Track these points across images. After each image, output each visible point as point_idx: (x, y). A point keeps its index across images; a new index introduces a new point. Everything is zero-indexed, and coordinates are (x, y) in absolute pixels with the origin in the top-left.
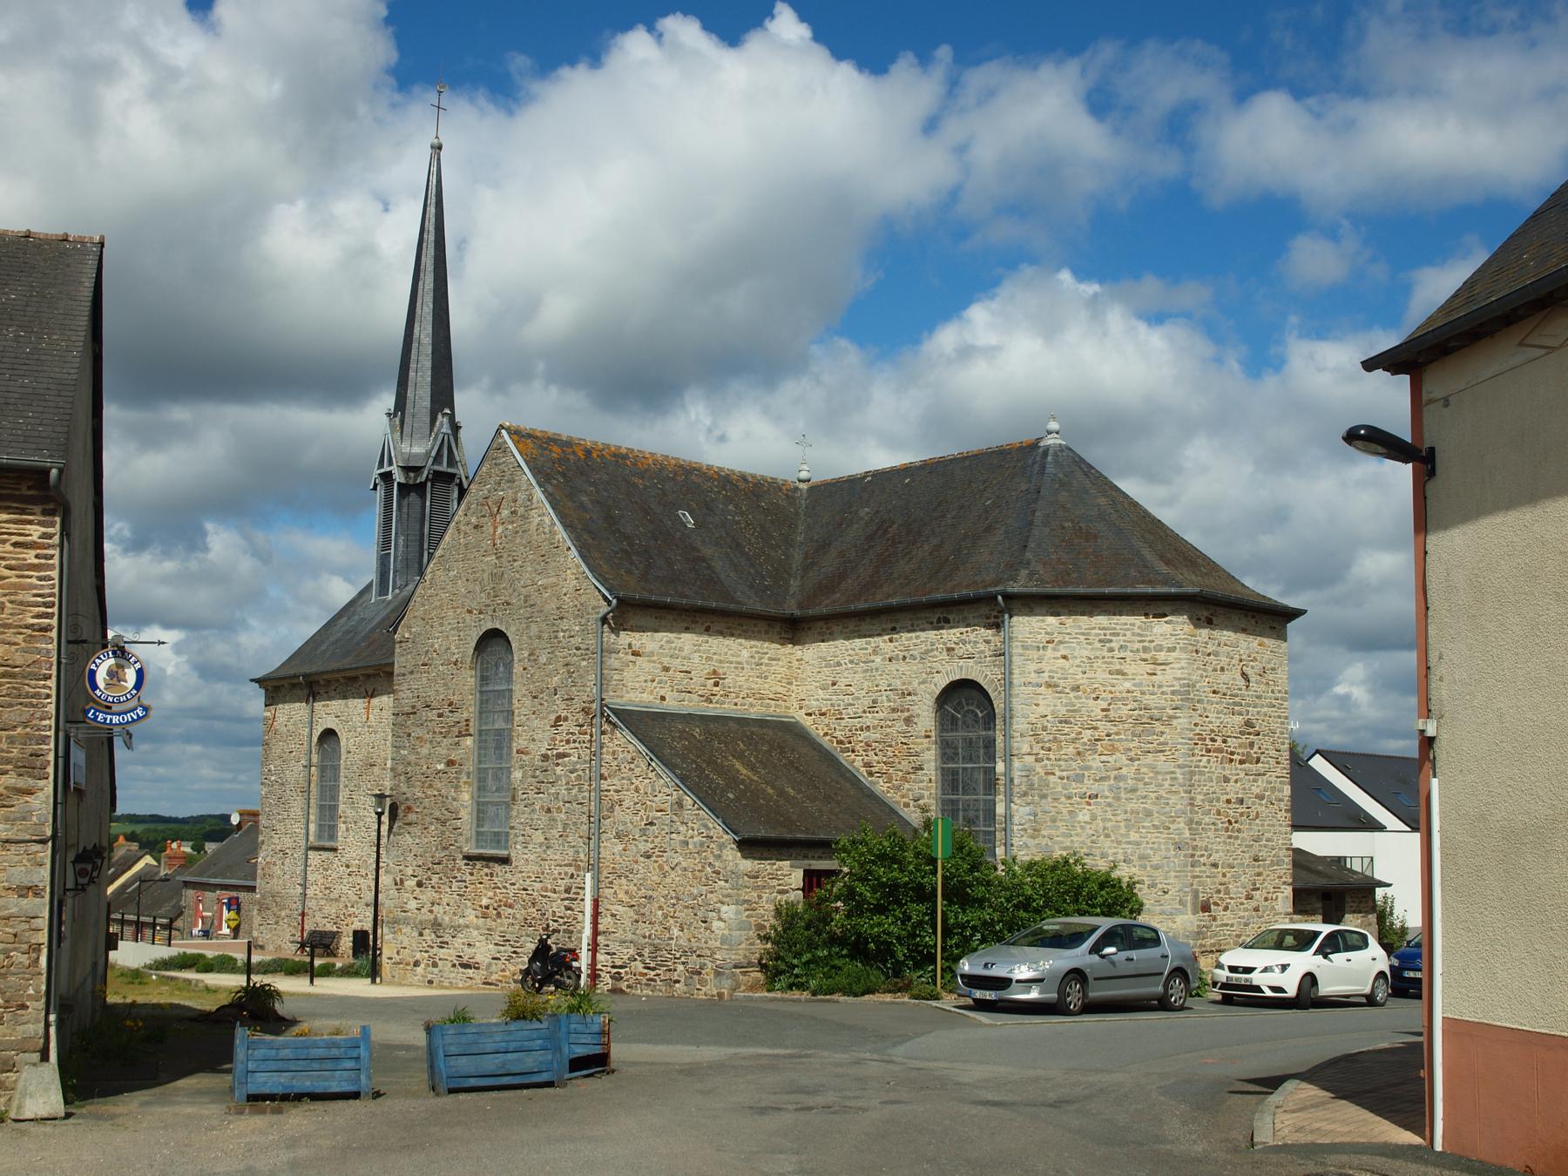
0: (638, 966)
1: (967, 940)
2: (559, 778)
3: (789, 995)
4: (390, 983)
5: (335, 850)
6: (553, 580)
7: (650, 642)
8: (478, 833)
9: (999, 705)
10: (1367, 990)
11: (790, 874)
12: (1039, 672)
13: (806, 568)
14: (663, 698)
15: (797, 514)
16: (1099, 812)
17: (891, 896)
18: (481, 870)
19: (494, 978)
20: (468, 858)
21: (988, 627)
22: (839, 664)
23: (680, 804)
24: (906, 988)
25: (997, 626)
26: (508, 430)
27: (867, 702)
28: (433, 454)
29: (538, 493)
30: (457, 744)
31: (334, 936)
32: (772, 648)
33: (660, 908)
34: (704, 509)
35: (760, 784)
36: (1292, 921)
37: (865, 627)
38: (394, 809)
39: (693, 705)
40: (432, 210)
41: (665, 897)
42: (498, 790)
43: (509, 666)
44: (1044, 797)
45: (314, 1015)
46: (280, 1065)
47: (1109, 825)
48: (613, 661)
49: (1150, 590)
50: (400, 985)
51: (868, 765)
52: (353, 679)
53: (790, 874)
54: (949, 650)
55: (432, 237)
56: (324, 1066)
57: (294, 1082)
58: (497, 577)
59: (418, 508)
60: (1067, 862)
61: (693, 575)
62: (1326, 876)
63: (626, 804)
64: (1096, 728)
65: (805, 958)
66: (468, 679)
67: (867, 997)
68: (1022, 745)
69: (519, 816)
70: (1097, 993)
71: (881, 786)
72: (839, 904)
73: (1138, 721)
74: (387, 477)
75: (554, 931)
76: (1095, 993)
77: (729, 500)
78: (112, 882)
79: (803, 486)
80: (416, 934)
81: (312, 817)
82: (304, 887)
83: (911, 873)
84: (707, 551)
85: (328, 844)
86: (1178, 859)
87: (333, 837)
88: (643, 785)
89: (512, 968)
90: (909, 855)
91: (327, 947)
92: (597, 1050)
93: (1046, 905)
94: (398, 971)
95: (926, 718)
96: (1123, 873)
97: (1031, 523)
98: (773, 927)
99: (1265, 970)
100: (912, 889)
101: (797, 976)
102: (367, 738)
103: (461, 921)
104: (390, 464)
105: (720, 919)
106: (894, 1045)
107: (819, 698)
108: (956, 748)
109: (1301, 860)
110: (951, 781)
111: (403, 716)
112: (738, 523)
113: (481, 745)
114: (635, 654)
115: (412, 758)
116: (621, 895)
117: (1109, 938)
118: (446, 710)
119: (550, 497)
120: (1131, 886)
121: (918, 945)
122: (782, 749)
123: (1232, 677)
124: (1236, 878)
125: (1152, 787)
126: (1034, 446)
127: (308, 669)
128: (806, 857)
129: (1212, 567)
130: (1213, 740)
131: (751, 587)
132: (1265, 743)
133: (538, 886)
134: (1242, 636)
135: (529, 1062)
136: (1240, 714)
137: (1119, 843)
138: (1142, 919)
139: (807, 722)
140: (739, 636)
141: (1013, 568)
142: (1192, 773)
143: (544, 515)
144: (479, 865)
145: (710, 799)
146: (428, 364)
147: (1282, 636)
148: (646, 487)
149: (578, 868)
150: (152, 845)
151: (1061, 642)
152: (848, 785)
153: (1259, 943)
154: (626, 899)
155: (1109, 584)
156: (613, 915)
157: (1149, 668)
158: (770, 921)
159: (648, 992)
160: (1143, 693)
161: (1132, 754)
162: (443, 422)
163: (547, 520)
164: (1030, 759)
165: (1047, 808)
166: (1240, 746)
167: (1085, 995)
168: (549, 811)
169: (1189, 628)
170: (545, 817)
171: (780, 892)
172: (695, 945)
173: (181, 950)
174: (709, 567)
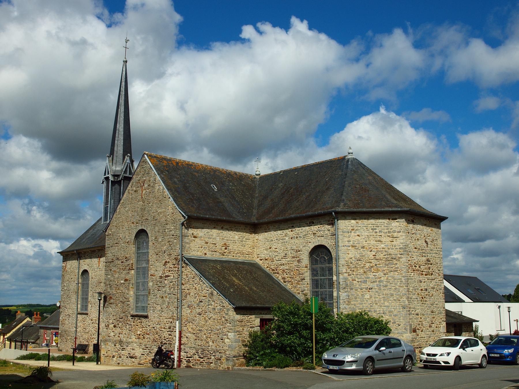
0: (197, 357)
1: (324, 345)
2: (166, 285)
3: (254, 368)
4: (104, 364)
5: (87, 314)
6: (164, 210)
7: (201, 232)
8: (136, 307)
9: (334, 254)
10: (479, 362)
11: (255, 321)
12: (349, 241)
13: (259, 206)
14: (205, 254)
15: (255, 186)
16: (373, 295)
17: (295, 329)
18: (138, 321)
19: (142, 362)
20: (133, 316)
21: (329, 224)
22: (272, 241)
23: (212, 294)
24: (301, 365)
25: (332, 224)
26: (147, 155)
27: (283, 254)
28: (124, 170)
29: (158, 178)
31: (86, 346)
32: (247, 235)
33: (205, 334)
35: (243, 287)
36: (446, 336)
37: (282, 226)
38: (105, 298)
39: (217, 256)
40: (123, 83)
41: (207, 330)
42: (143, 290)
43: (147, 243)
44: (352, 289)
45: (68, 379)
47: (377, 299)
48: (186, 240)
49: (390, 209)
50: (107, 365)
51: (284, 278)
53: (255, 321)
54: (314, 234)
58: (143, 210)
60: (361, 314)
61: (217, 208)
62: (455, 318)
63: (191, 294)
64: (371, 263)
65: (261, 353)
66: (133, 248)
67: (286, 369)
69: (152, 299)
70: (379, 366)
71: (289, 286)
72: (274, 331)
74: (107, 179)
75: (165, 344)
76: (378, 366)
77: (230, 181)
81: (79, 302)
82: (76, 328)
83: (302, 319)
84: (222, 199)
85: (85, 312)
86: (404, 312)
87: (86, 309)
88: (198, 287)
89: (149, 358)
91: (84, 350)
93: (354, 331)
94: (107, 359)
95: (306, 260)
97: (344, 186)
98: (248, 341)
99: (441, 355)
100: (303, 325)
101: (258, 360)
102: (99, 273)
103: (130, 340)
104: (108, 174)
105: (228, 338)
107: (264, 254)
108: (317, 271)
109: (448, 313)
110: (315, 284)
111: (109, 263)
112: (234, 189)
113: (138, 273)
114: (195, 237)
115: (112, 278)
116: (190, 330)
117: (381, 344)
118: (124, 260)
119: (162, 179)
120: (386, 324)
121: (305, 347)
122: (251, 273)
123: (422, 243)
124: (425, 319)
125: (393, 285)
126: (344, 158)
127: (77, 248)
128: (261, 314)
130: (415, 266)
131: (239, 212)
132: (434, 268)
133: (158, 326)
134: (424, 227)
137: (381, 306)
138: (391, 335)
139: (260, 263)
140: (234, 231)
141: (338, 203)
142: (408, 279)
143: (161, 186)
144: (136, 319)
145: (224, 292)
146: (122, 138)
147: (439, 228)
148: (199, 176)
149: (173, 319)
150: (30, 314)
151: (357, 230)
152: (276, 286)
154: (192, 331)
155: (375, 207)
156: (187, 337)
157: (391, 239)
158: (247, 339)
159: (200, 367)
160: (389, 249)
161: (385, 272)
163: (161, 187)
164: (346, 275)
165: (353, 293)
166: (425, 269)
167: (374, 367)
168: (162, 297)
169: (405, 224)
171: (251, 327)
172: (218, 348)
173: (31, 352)
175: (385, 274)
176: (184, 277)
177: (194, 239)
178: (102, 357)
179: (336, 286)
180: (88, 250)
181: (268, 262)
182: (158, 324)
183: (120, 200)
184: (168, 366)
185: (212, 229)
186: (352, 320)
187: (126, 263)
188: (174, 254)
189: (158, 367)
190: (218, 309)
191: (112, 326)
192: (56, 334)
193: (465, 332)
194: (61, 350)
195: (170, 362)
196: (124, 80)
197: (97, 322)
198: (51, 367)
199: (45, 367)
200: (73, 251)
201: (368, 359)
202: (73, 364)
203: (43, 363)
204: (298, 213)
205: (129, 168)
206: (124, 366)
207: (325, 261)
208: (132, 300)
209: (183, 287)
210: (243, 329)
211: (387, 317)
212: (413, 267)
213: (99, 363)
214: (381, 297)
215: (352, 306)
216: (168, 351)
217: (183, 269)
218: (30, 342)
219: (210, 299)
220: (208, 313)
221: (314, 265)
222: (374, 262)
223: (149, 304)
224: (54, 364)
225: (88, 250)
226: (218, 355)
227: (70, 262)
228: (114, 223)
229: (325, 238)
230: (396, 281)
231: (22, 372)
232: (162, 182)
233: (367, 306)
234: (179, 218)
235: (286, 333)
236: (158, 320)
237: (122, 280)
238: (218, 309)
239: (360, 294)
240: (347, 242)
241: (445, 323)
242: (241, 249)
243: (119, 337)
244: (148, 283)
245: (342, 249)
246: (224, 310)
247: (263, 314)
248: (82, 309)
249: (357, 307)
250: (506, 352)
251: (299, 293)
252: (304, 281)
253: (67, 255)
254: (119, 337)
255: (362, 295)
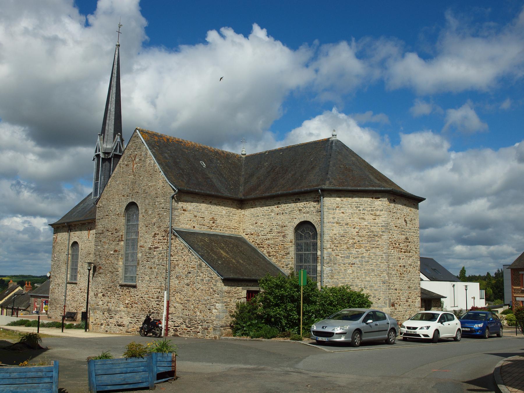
0: (184, 326)
1: (310, 317)
2: (155, 256)
3: (242, 338)
5: (76, 284)
6: (154, 183)
7: (190, 206)
9: (318, 230)
10: (455, 336)
11: (242, 292)
12: (334, 218)
14: (194, 227)
15: (241, 165)
19: (130, 330)
20: (121, 286)
21: (315, 201)
22: (258, 216)
23: (200, 265)
24: (288, 336)
25: (318, 201)
26: (139, 130)
27: (269, 230)
28: (114, 148)
29: (149, 152)
30: (118, 244)
32: (234, 210)
33: (193, 304)
34: (209, 161)
35: (232, 260)
37: (268, 202)
38: (95, 268)
39: (205, 230)
40: (116, 66)
42: (132, 261)
43: (137, 215)
44: (335, 264)
46: (11, 381)
47: (359, 274)
48: (176, 213)
49: (374, 189)
50: (96, 332)
51: (268, 253)
52: (84, 224)
53: (242, 292)
54: (300, 210)
55: (115, 75)
56: (34, 381)
57: (18, 390)
58: (134, 183)
59: (108, 167)
61: (205, 183)
64: (354, 239)
65: (248, 324)
66: (122, 220)
67: (273, 339)
68: (327, 245)
69: (140, 270)
71: (273, 260)
73: (369, 237)
74: (98, 156)
75: (153, 313)
76: (365, 338)
78: (7, 295)
79: (243, 156)
80: (101, 313)
81: (69, 272)
82: (65, 296)
84: (211, 175)
85: (74, 282)
86: (384, 287)
87: (76, 279)
88: (187, 259)
89: (137, 327)
90: (288, 285)
91: (72, 318)
92: (170, 369)
95: (291, 235)
96: (365, 292)
97: (329, 165)
98: (235, 312)
99: (421, 328)
101: (245, 331)
102: (88, 245)
104: (99, 151)
105: (216, 309)
106: (297, 362)
107: (250, 229)
108: (302, 246)
110: (300, 258)
111: (99, 234)
112: (221, 167)
113: (127, 245)
114: (184, 210)
115: (102, 249)
116: (178, 300)
117: (368, 317)
121: (291, 319)
123: (401, 222)
124: (403, 294)
125: (374, 261)
127: (68, 221)
128: (247, 286)
129: (393, 184)
130: (395, 244)
131: (226, 188)
132: (411, 245)
133: (146, 296)
134: (404, 207)
135: (137, 377)
136: (404, 235)
137: (362, 281)
139: (246, 237)
140: (222, 206)
141: (323, 181)
142: (389, 256)
143: (151, 160)
144: (125, 288)
145: (212, 264)
146: (113, 118)
147: (417, 208)
149: (162, 289)
151: (341, 207)
153: (415, 318)
154: (179, 301)
155: (360, 186)
156: (175, 307)
157: (373, 217)
158: (234, 310)
161: (367, 248)
162: (118, 138)
163: (152, 162)
164: (330, 250)
165: (336, 268)
166: (404, 246)
167: (361, 339)
168: (151, 268)
169: (387, 203)
170: (149, 270)
172: (205, 318)
173: (21, 319)
174: (211, 181)
175: (367, 251)
176: (173, 248)
177: (183, 212)
178: (90, 325)
179: (320, 261)
180: (78, 223)
181: (253, 237)
182: (147, 293)
183: (110, 176)
184: (156, 335)
185: (201, 203)
186: (336, 293)
187: (116, 235)
188: (164, 227)
189: (146, 335)
190: (206, 280)
191: (100, 295)
192: (46, 303)
193: (434, 307)
194: (50, 318)
195: (158, 330)
196: (116, 63)
197: (86, 291)
198: (41, 334)
199: (36, 334)
200: (64, 223)
201: (356, 331)
202: (62, 331)
203: (33, 330)
204: (285, 190)
205: (119, 147)
206: (112, 334)
207: (310, 236)
208: (121, 270)
209: (172, 258)
210: (231, 300)
211: (368, 291)
212: (394, 244)
213: (88, 330)
214: (362, 272)
215: (335, 280)
216: (157, 320)
217: (173, 241)
218: (20, 310)
219: (198, 271)
220: (196, 284)
221: (298, 240)
222: (357, 238)
223: (137, 275)
224: (43, 331)
225: (78, 223)
226: (205, 325)
227: (61, 234)
228: (105, 195)
229: (310, 215)
230: (377, 257)
231: (11, 338)
232: (153, 156)
233: (349, 281)
234: (169, 191)
235: (272, 305)
236: (146, 289)
237: (111, 251)
238: (206, 280)
239: (343, 269)
240: (331, 219)
241: (420, 298)
242: (228, 223)
243: (107, 305)
244: (137, 254)
245: (327, 226)
246: (213, 281)
247: (250, 286)
248: (71, 279)
249: (340, 281)
250: (476, 326)
251: (283, 267)
252: (288, 255)
253: (57, 228)
254: (107, 305)
255: (345, 270)
